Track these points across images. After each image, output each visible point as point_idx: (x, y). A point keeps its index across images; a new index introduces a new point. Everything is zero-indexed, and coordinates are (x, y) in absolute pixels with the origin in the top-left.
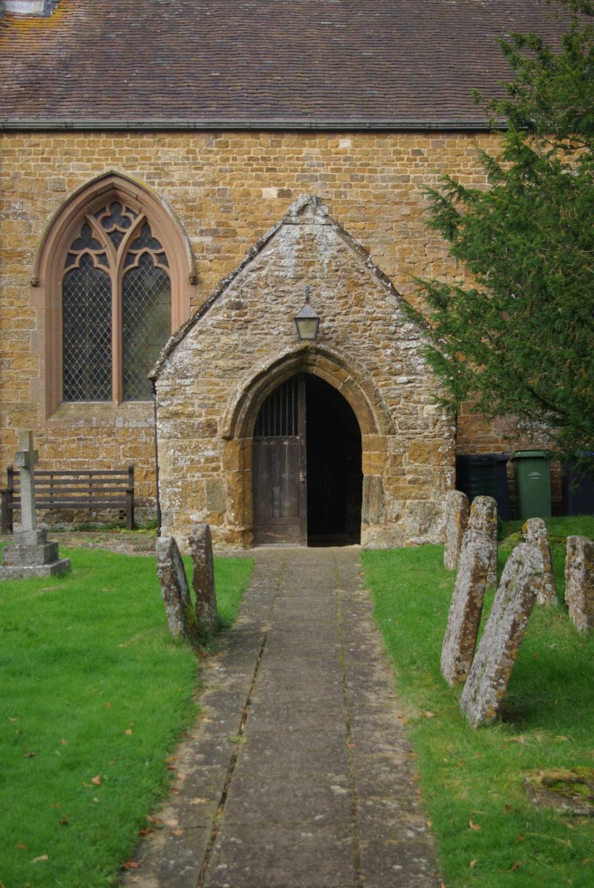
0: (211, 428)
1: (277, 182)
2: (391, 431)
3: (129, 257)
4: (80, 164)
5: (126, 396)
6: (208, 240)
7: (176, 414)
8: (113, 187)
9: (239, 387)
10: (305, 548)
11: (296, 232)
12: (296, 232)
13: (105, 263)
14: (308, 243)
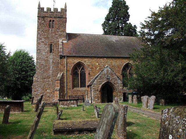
0: (98, 90)
1: (98, 63)
2: (116, 90)
3: (81, 71)
4: (76, 61)
5: (81, 87)
6: (90, 69)
7: (94, 89)
8: (80, 63)
9: (101, 85)
10: (107, 103)
11: (106, 69)
12: (106, 69)
13: (78, 72)
14: (108, 70)
